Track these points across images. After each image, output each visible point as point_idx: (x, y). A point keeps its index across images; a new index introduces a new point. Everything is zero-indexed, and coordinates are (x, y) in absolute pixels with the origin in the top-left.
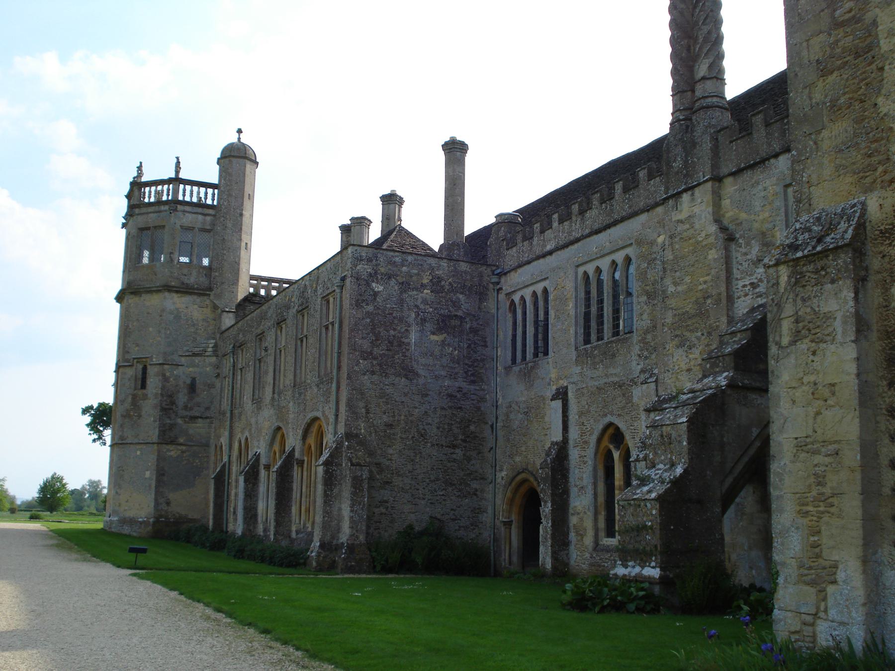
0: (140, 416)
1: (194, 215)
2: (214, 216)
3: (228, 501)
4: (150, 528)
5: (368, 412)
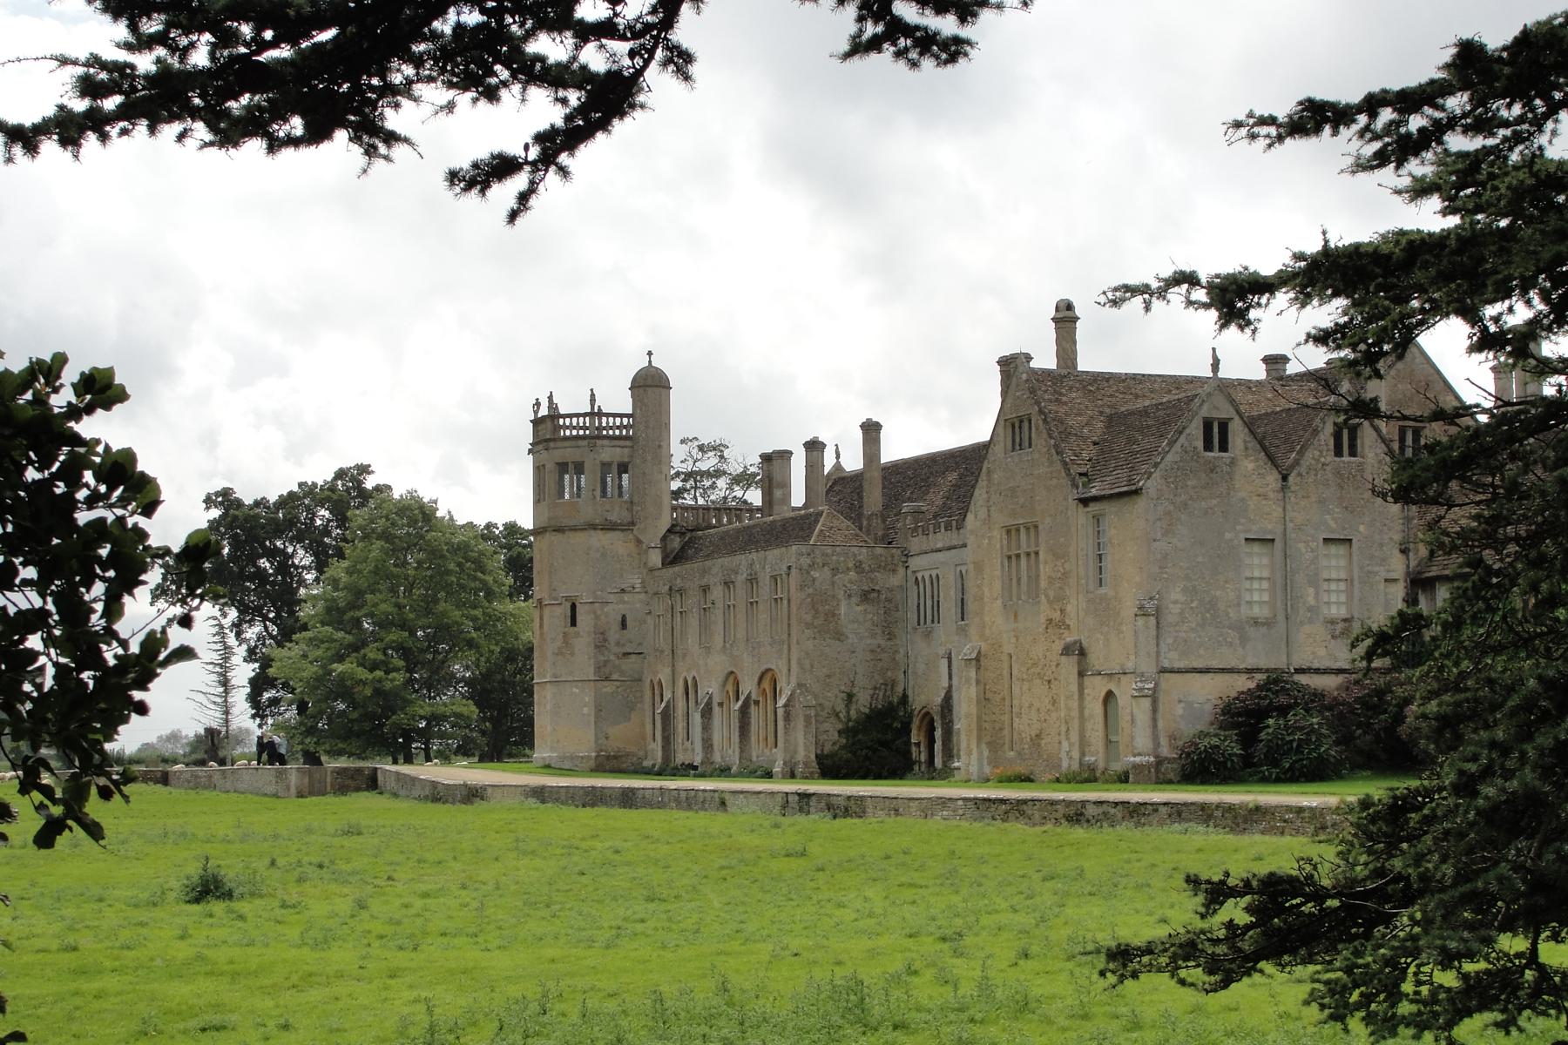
0: (572, 654)
2: (632, 447)
5: (812, 666)
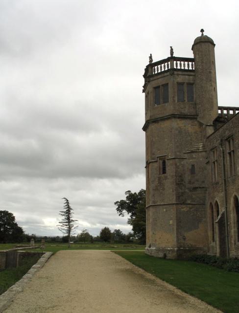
0: (164, 189)
1: (184, 76)
2: (194, 75)
3: (228, 237)
4: (175, 254)
